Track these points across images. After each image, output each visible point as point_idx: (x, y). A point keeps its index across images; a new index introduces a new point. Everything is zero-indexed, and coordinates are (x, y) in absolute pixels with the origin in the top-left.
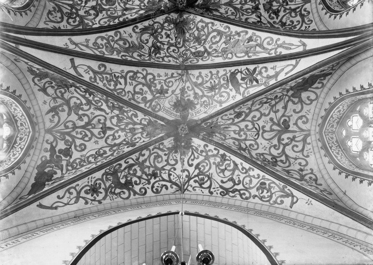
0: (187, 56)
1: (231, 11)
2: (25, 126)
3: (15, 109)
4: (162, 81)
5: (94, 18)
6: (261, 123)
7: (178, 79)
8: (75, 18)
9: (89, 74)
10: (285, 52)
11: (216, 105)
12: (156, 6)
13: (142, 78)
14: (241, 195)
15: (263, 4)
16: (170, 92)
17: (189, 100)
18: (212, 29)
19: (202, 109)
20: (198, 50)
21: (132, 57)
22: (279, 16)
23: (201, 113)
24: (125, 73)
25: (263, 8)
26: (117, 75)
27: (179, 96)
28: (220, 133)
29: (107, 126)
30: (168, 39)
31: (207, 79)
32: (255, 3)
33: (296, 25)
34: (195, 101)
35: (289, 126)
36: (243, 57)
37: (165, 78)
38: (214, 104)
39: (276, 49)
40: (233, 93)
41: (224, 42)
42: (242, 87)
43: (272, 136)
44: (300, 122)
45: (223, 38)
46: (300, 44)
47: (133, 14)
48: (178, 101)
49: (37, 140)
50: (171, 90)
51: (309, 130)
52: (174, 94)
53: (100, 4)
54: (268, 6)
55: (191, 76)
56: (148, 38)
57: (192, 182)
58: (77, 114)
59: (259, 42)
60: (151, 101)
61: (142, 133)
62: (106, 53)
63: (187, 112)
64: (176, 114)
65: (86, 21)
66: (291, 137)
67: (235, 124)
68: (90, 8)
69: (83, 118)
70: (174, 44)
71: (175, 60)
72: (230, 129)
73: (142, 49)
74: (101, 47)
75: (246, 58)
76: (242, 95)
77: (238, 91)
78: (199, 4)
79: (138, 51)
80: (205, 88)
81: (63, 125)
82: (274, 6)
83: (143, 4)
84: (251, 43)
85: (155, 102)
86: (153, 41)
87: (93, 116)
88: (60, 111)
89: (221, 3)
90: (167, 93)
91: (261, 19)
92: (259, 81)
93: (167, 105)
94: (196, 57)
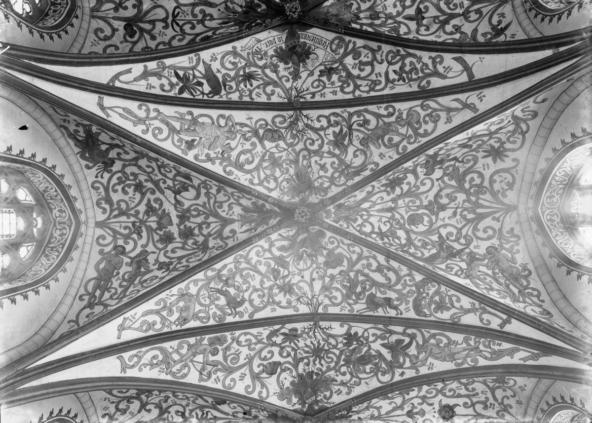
0: (292, 132)
1: (223, 211)
4: (330, 86)
5: (440, 190)
6: (170, 32)
7: (304, 91)
8: (471, 188)
9: (444, 67)
10: (133, 105)
11: (241, 51)
12: (343, 215)
13: (361, 85)
15: (172, 225)
16: (317, 73)
17: (286, 63)
18: (252, 175)
19: (264, 48)
20: (274, 144)
21: (378, 116)
22: (146, 205)
23: (266, 41)
24: (389, 86)
25: (172, 218)
26: (401, 82)
27: (301, 69)
28: (235, 12)
29: (415, 22)
30: (322, 162)
31: (257, 90)
32: (185, 226)
33: (119, 184)
34: (276, 61)
35: (125, 28)
36: (202, 115)
37: (325, 90)
38: (246, 52)
39: (147, 117)
40: (215, 66)
41: (232, 150)
42: (201, 73)
43: (152, 13)
44: (108, 31)
45: (235, 158)
46: (109, 112)
47: (379, 201)
48: (304, 61)
50: (316, 77)
51: (93, 17)
52: (309, 71)
53: (433, 215)
54: (164, 221)
55: (283, 94)
56: (354, 160)
58: (462, 33)
59: (176, 138)
60: (345, 55)
61: (359, 8)
62: (419, 109)
63: (288, 44)
64: (305, 40)
65: (453, 183)
66: (121, 10)
67: (211, 29)
68: (449, 206)
69: (454, 30)
70: (312, 155)
71: (310, 122)
72: (220, 21)
73: (364, 138)
74: (427, 119)
75: (197, 112)
76: (201, 61)
77: (208, 68)
78: (275, 219)
79: (370, 132)
80: (260, 78)
81: (484, 14)
82: (154, 221)
83: (365, 217)
84: (189, 139)
85: (339, 54)
86: (346, 157)
87: (437, 34)
88: (489, 33)
89: (240, 223)
90: (320, 71)
91: (175, 198)
92: (173, 74)
93: (320, 53)
94: (276, 131)
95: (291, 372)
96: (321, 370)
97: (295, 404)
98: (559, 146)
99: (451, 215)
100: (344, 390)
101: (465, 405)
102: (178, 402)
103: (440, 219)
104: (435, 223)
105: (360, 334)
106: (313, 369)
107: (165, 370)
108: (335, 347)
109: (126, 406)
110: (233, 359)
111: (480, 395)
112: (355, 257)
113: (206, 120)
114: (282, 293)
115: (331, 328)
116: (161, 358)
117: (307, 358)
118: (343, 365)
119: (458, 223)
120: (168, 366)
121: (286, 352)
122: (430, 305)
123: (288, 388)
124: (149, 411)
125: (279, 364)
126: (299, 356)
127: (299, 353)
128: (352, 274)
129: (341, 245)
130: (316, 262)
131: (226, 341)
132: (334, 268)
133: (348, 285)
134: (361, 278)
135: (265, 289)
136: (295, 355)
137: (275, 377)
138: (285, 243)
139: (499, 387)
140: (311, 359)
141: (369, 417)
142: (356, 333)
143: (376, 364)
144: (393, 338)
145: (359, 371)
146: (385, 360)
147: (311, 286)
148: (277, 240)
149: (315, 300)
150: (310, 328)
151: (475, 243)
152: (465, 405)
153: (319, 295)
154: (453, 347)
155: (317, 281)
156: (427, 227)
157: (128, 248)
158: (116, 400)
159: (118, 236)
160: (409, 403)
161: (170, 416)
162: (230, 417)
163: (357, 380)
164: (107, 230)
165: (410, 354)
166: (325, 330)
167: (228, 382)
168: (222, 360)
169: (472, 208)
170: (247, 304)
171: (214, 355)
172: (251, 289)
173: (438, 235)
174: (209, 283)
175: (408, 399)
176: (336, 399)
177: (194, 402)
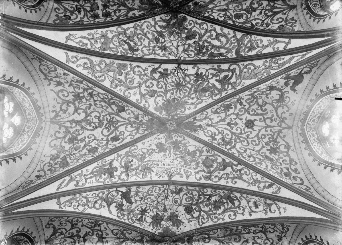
1: (129, 3)
2: (311, 134)
3: (319, 149)
15: (99, 10)
25: (99, 6)
32: (106, 11)
49: (300, 120)
53: (248, 14)
83: (210, 13)
89: (138, 10)
95: (163, 98)
96: (180, 97)
97: (164, 115)
98: (319, 93)
99: (259, 14)
100: (193, 107)
101: (260, 120)
102: (97, 109)
103: (253, 16)
104: (250, 18)
105: (204, 74)
106: (175, 96)
107: (92, 73)
108: (189, 83)
109: (67, 108)
110: (130, 81)
111: (269, 113)
112: (203, 32)
114: (161, 50)
115: (187, 70)
116: (89, 65)
117: (172, 89)
118: (193, 94)
119: (262, 18)
120: (93, 72)
121: (160, 85)
122: (245, 50)
123: (160, 106)
124: (79, 114)
125: (156, 91)
126: (168, 88)
127: (168, 86)
128: (201, 43)
129: (196, 25)
130: (181, 37)
132: (191, 40)
133: (199, 48)
134: (206, 44)
135: (151, 47)
136: (166, 87)
137: (153, 99)
138: (164, 24)
139: (280, 106)
140: (175, 91)
141: (206, 124)
142: (202, 73)
143: (212, 92)
144: (222, 75)
145: (202, 96)
146: (217, 88)
147: (177, 49)
148: (159, 21)
149: (179, 55)
150: (175, 70)
151: (272, 25)
152: (260, 120)
153: (181, 53)
154: (257, 70)
155: (180, 46)
156: (245, 20)
157: (72, 17)
158: (61, 101)
159: (67, 11)
160: (229, 118)
161: (91, 118)
162: (126, 121)
163: (201, 101)
164: (61, 6)
165: (231, 82)
166: (184, 71)
167: (126, 93)
168: (123, 79)
169: (270, 9)
170: (140, 52)
171: (119, 75)
172: (143, 46)
173: (251, 24)
174: (119, 35)
175: (228, 115)
176: (188, 112)
177: (106, 110)
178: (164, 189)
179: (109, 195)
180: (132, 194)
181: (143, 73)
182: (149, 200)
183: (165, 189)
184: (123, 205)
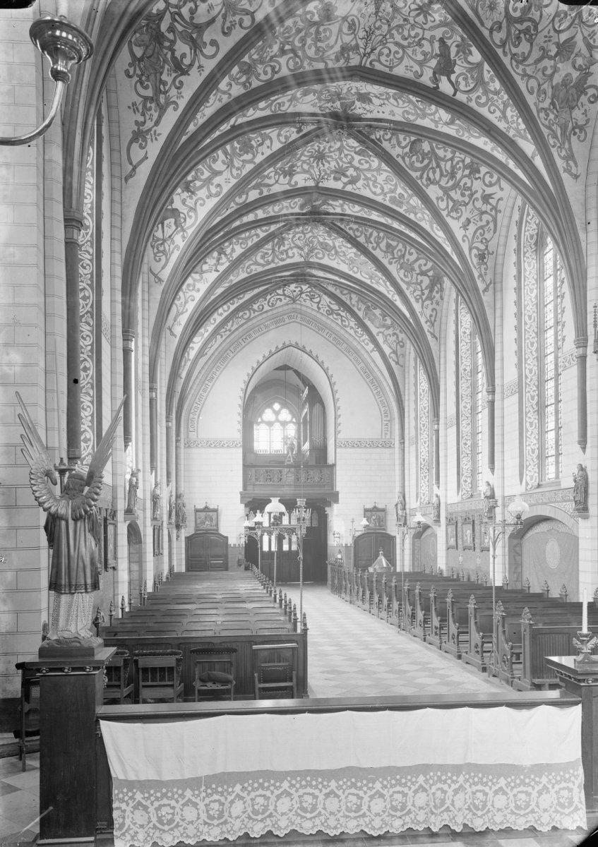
14: (342, 321)
57: (303, 295)
75: (368, 282)
105: (282, 177)
108: (304, 162)
113: (365, 275)
117: (331, 152)
125: (355, 153)
131: (391, 197)
140: (327, 150)
142: (285, 177)
178: (373, 57)
179: (472, 86)
180: (433, 63)
181: (371, 183)
182: (406, 33)
183: (369, 54)
184: (457, 46)
